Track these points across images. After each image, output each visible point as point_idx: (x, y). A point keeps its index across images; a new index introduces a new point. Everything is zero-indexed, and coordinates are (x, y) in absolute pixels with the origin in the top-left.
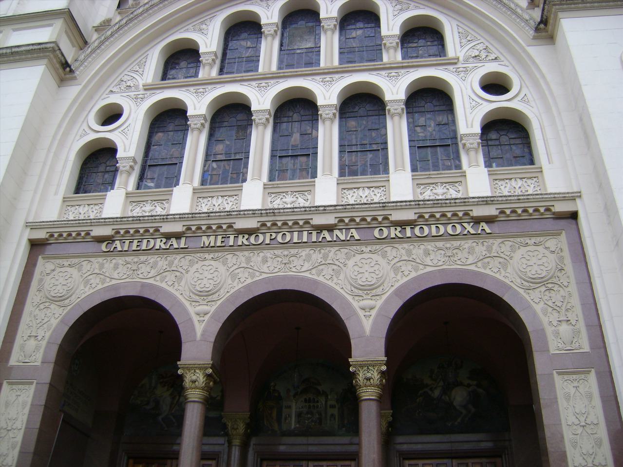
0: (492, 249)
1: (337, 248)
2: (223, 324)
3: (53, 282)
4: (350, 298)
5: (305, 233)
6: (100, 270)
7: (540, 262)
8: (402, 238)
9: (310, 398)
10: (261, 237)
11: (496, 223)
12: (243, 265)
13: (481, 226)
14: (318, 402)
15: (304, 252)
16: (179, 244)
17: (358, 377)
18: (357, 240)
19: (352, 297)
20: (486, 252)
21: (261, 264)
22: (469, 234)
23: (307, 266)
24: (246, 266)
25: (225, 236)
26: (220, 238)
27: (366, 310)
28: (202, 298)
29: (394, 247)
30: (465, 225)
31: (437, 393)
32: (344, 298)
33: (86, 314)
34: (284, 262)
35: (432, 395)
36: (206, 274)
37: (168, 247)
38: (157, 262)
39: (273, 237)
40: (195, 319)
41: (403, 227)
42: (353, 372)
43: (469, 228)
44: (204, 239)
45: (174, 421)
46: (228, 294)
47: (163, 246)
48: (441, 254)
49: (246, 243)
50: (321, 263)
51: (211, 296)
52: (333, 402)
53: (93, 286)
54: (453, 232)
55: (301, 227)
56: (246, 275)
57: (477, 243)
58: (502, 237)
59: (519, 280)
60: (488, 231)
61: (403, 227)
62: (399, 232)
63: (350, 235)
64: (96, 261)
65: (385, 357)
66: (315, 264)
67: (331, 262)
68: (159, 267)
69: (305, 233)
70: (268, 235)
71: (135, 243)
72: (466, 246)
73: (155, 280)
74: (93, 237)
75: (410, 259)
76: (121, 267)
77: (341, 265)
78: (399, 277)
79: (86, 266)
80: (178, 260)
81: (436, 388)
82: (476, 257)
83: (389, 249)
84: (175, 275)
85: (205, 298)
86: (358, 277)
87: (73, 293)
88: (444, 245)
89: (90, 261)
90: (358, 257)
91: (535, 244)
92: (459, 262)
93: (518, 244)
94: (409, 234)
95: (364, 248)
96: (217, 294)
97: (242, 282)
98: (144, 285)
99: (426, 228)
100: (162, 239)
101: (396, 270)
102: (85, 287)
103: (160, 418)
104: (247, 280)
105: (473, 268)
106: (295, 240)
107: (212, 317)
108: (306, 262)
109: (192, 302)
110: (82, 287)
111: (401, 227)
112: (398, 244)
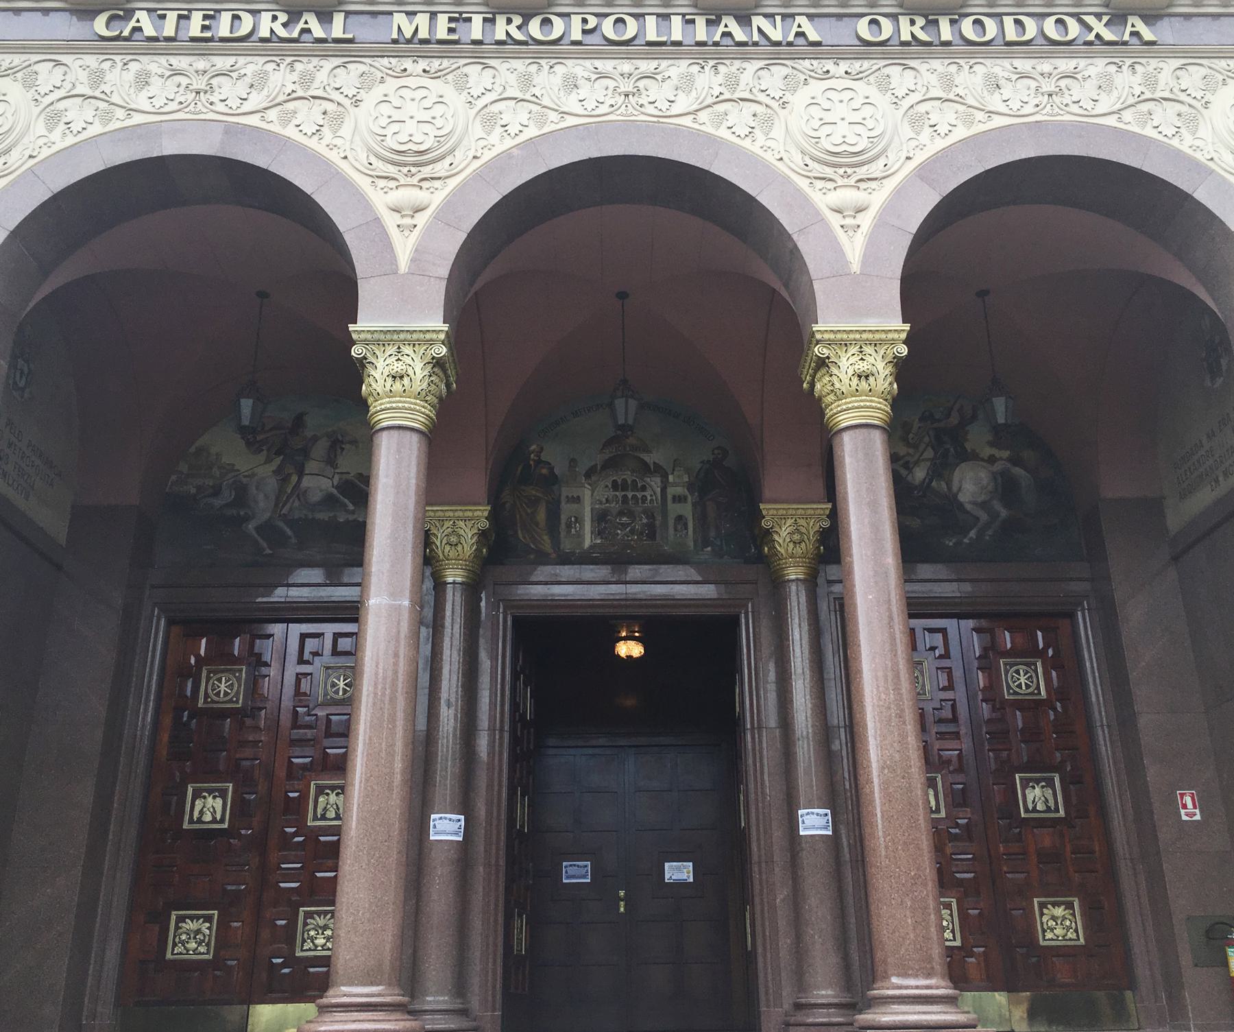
1: (762, 63)
3: (386, 114)
7: (857, 117)
9: (624, 480)
10: (558, 26)
13: (796, 24)
14: (644, 488)
15: (677, 69)
16: (328, 30)
17: (373, 372)
18: (150, 39)
21: (562, 93)
23: (256, 101)
24: (89, 92)
25: (457, 15)
28: (405, 170)
30: (1090, 20)
32: (787, 180)
33: (56, 198)
35: (909, 478)
36: (411, 108)
37: (295, 34)
39: (590, 26)
40: (391, 221)
44: (400, 19)
45: (289, 532)
46: (477, 163)
47: (282, 33)
49: (518, 35)
50: (294, 95)
52: (679, 490)
53: (75, 127)
54: (977, 35)
57: (278, 65)
58: (1185, 54)
59: (798, 158)
60: (813, 36)
61: (930, 17)
62: (922, 28)
63: (795, 29)
64: (80, 62)
67: (320, 93)
70: (576, 21)
71: (197, 20)
72: (250, 70)
76: (154, 80)
77: (346, 102)
79: (48, 75)
80: (324, 71)
81: (917, 463)
82: (1119, 98)
83: (895, 71)
84: (322, 109)
87: (14, 145)
89: (58, 63)
90: (391, 84)
95: (829, 65)
97: (75, 132)
98: (232, 131)
101: (917, 122)
103: (251, 526)
105: (1111, 121)
106: (652, 36)
107: (437, 217)
109: (376, 180)
111: (926, 16)
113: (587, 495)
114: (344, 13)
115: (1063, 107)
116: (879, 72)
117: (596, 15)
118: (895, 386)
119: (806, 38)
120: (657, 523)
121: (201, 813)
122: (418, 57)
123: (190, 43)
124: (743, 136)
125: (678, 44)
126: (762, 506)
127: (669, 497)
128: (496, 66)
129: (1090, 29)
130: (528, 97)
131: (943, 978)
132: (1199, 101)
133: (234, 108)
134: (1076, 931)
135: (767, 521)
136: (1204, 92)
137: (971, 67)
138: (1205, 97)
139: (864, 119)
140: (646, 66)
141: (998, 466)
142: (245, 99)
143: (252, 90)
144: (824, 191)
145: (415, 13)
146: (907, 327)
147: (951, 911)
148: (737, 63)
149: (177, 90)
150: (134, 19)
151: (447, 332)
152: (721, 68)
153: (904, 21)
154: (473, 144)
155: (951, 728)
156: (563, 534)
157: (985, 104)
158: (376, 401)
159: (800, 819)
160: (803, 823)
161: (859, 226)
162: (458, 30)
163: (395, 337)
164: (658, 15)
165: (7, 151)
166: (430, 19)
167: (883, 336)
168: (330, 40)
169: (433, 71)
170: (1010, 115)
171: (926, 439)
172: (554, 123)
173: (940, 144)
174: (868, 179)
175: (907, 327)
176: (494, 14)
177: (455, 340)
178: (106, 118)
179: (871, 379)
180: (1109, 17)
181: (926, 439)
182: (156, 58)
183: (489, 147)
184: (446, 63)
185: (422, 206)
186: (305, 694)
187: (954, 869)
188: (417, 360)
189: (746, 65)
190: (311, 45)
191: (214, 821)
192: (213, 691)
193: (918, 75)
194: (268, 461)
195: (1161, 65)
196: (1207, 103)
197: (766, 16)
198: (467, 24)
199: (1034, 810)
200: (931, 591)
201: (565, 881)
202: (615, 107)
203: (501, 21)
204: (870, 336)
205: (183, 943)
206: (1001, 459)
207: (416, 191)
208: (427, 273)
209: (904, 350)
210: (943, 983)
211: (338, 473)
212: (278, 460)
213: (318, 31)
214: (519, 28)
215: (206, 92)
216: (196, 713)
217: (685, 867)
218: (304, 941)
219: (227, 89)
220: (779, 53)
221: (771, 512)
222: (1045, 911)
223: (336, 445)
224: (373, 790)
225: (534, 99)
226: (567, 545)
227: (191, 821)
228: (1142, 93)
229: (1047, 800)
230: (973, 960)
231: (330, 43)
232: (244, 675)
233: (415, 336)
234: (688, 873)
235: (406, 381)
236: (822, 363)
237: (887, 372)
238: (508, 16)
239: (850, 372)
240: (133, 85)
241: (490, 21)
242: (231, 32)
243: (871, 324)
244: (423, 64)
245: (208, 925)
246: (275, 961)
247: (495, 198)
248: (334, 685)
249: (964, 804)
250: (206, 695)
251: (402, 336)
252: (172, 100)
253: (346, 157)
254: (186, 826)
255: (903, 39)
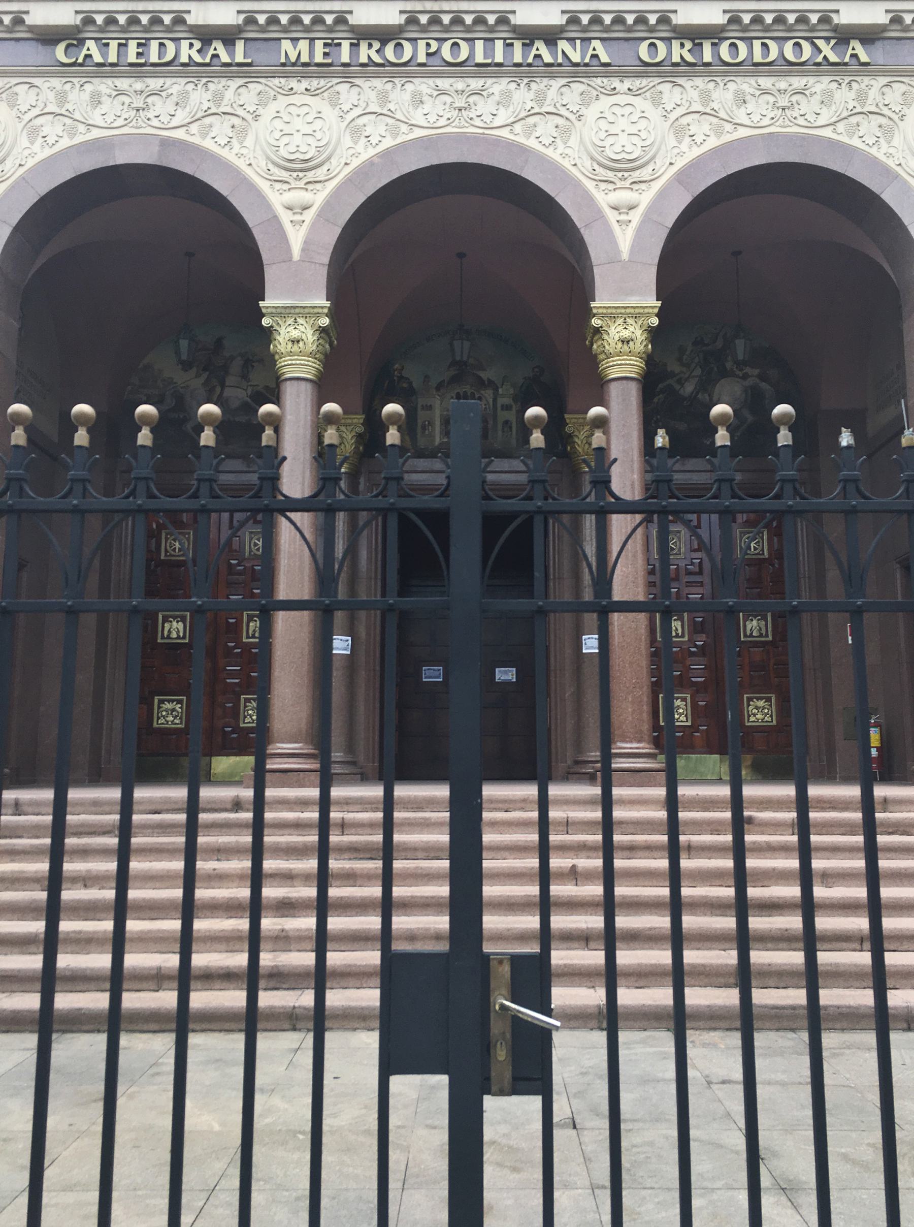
0: (867, 98)
1: (564, 81)
2: (345, 229)
3: (279, 128)
4: (590, 185)
5: (499, 44)
6: (60, 105)
8: (694, 65)
11: (879, 44)
12: (51, 108)
15: (498, 86)
16: (232, 54)
17: (278, 337)
19: (269, 183)
20: (855, 104)
21: (89, 108)
22: (825, 63)
23: (181, 117)
25: (330, 41)
26: (319, 44)
27: (621, 211)
28: (295, 174)
29: (676, 84)
30: (820, 43)
31: (689, 388)
32: (578, 184)
34: (457, 105)
35: (681, 392)
37: (208, 60)
38: (187, 92)
39: (432, 50)
40: (285, 217)
41: (697, 41)
42: (598, 328)
43: (827, 50)
44: (286, 45)
46: (348, 170)
47: (198, 58)
48: (768, 103)
49: (377, 59)
50: (532, 112)
51: (313, 172)
53: (51, 140)
54: (796, 57)
55: (491, 29)
56: (382, 129)
57: (196, 85)
58: (885, 73)
60: (605, 58)
61: (697, 41)
62: (689, 51)
63: (590, 52)
64: (48, 84)
65: (657, 300)
66: (196, 112)
67: (551, 109)
68: (192, 104)
69: (499, 44)
70: (422, 44)
72: (175, 89)
73: (511, 131)
74: (32, 29)
75: (708, 110)
77: (572, 117)
78: (684, 147)
81: (687, 380)
82: (836, 112)
84: (231, 123)
85: (626, 174)
86: (607, 143)
88: (773, 85)
89: (32, 86)
90: (283, 101)
91: (628, 92)
92: (801, 121)
93: (274, 90)
94: (708, 57)
95: (616, 83)
96: (325, 168)
98: (166, 143)
99: (742, 47)
100: (192, 41)
101: (679, 131)
102: (32, 143)
104: (383, 140)
105: (827, 133)
106: (480, 58)
107: (320, 214)
108: (180, 110)
110: (25, 142)
111: (692, 40)
112: (686, 78)
113: (437, 403)
114: (243, 41)
115: (793, 120)
116: (654, 89)
117: (436, 39)
118: (650, 346)
119: (599, 60)
120: (490, 426)
121: (169, 631)
122: (301, 77)
123: (128, 68)
124: (547, 145)
125: (499, 65)
126: (566, 416)
127: (499, 406)
128: (361, 85)
129: (820, 51)
130: (385, 112)
131: (648, 743)
132: (897, 114)
133: (166, 123)
134: (771, 716)
135: (570, 427)
136: (902, 106)
137: (725, 84)
138: (903, 111)
139: (639, 131)
140: (476, 84)
141: (749, 382)
142: (173, 115)
143: (178, 107)
144: (606, 192)
145: (298, 39)
146: (659, 304)
147: (686, 702)
148: (545, 81)
149: (122, 107)
150: (86, 48)
151: (329, 308)
152: (533, 85)
153: (676, 44)
154: (345, 152)
155: (698, 578)
156: (418, 436)
157: (733, 117)
158: (281, 358)
159: (584, 642)
160: (586, 644)
161: (630, 221)
162: (331, 54)
163: (293, 311)
164: (485, 39)
165: (4, 160)
166: (310, 44)
167: (641, 311)
168: (234, 64)
169: (312, 90)
170: (751, 127)
171: (696, 360)
172: (407, 135)
173: (697, 152)
174: (640, 182)
175: (659, 304)
176: (358, 40)
177: (333, 314)
178: (72, 134)
179: (631, 343)
180: (836, 40)
181: (696, 360)
182: (104, 80)
183: (356, 155)
184: (322, 82)
185: (308, 206)
186: (236, 551)
187: (691, 675)
188: (308, 328)
189: (552, 82)
190: (219, 68)
191: (178, 637)
192: (171, 547)
193: (684, 91)
194: (198, 376)
195: (873, 82)
196: (903, 116)
197: (568, 39)
198: (338, 48)
199: (751, 635)
200: (690, 479)
201: (424, 680)
202: (451, 120)
203: (364, 45)
204: (632, 311)
205: (164, 716)
206: (752, 376)
207: (303, 193)
208: (314, 261)
209: (655, 321)
210: (647, 746)
211: (251, 386)
212: (205, 375)
213: (225, 58)
214: (377, 51)
215: (144, 109)
216: (161, 563)
217: (510, 671)
218: (245, 717)
219: (159, 106)
220: (578, 73)
221: (573, 421)
222: (751, 703)
223: (248, 363)
224: (291, 627)
225: (389, 113)
226: (422, 442)
227: (163, 637)
228: (854, 107)
229: (760, 629)
230: (698, 734)
231: (234, 66)
232: (192, 537)
233: (306, 310)
234: (512, 675)
235: (301, 344)
236: (597, 331)
237: (643, 338)
238: (369, 41)
239: (617, 338)
240: (89, 103)
241: (355, 46)
242: (159, 59)
243: (633, 301)
244: (305, 84)
245: (179, 706)
246: (226, 729)
247: (362, 199)
248: (256, 545)
249: (702, 631)
250: (166, 551)
251: (297, 311)
252: (119, 116)
253: (250, 165)
254: (159, 641)
255: (674, 61)
